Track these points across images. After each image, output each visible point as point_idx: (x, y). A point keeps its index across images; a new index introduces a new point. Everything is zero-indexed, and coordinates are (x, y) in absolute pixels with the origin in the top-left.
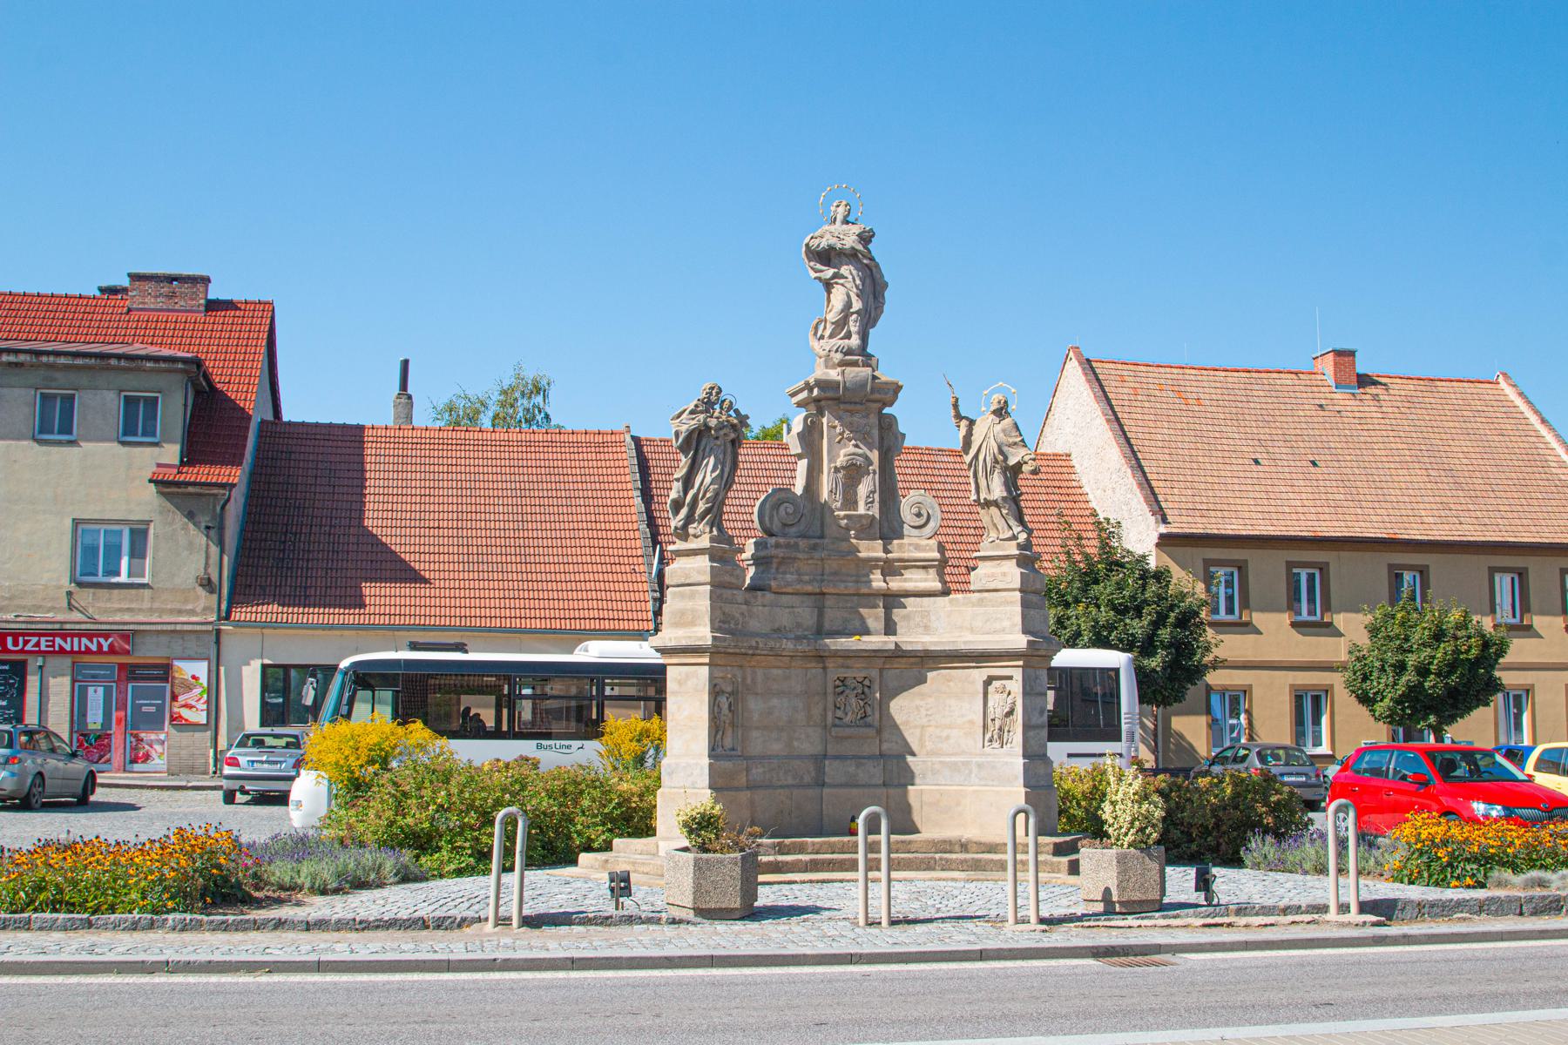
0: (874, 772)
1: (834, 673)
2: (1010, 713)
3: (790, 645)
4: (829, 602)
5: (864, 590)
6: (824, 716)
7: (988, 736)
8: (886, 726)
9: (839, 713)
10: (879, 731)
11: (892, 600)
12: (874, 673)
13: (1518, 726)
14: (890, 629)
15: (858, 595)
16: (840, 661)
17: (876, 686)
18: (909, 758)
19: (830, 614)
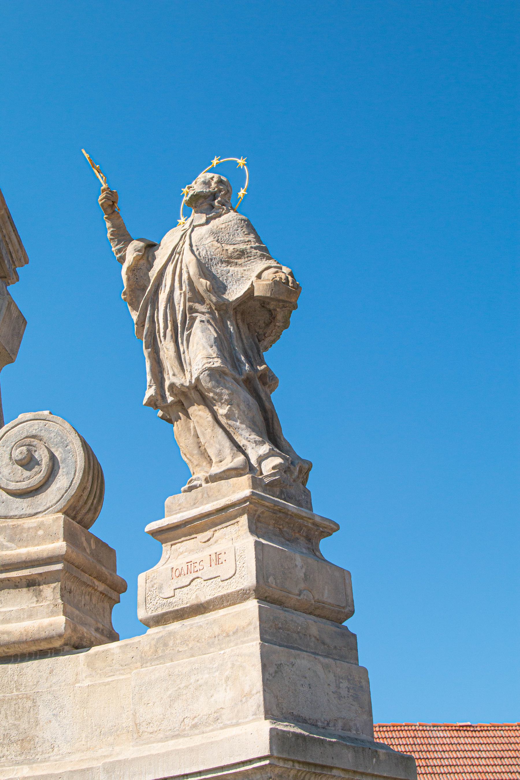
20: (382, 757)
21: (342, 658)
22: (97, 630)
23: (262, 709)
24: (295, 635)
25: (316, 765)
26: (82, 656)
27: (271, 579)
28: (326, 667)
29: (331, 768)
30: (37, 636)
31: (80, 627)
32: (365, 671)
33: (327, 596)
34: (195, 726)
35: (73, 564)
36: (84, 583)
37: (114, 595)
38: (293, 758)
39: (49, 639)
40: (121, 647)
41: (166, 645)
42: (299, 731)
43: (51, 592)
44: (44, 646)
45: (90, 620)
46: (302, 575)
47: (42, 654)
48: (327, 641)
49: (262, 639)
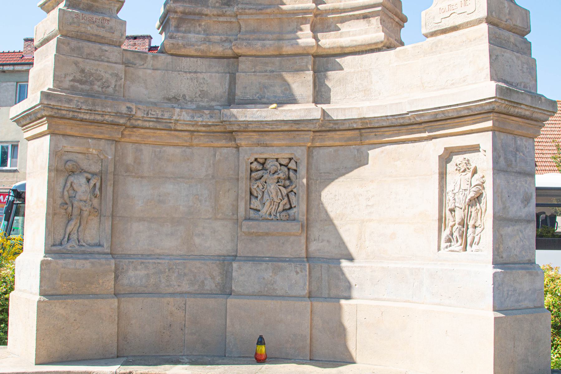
0: (295, 279)
1: (249, 153)
2: (477, 199)
3: (186, 116)
4: (244, 64)
5: (287, 49)
6: (236, 208)
7: (445, 234)
8: (315, 220)
9: (256, 204)
10: (307, 227)
11: (323, 62)
12: (300, 153)
13: (115, 264)
14: (320, 95)
15: (280, 55)
16: (255, 136)
17: (302, 171)
18: (345, 263)
19: (242, 79)
20: (543, 101)
21: (525, 53)
22: (396, 40)
23: (489, 76)
24: (504, 42)
25: (514, 102)
26: (392, 52)
27: (494, 13)
28: (518, 58)
29: (521, 104)
30: (370, 42)
31: (390, 38)
32: (535, 60)
33: (519, 23)
34: (453, 84)
35: (385, 7)
36: (390, 17)
37: (401, 23)
38: (505, 98)
39: (376, 44)
40: (412, 47)
41: (437, 46)
42: (505, 86)
43: (375, 21)
44: (373, 47)
45: (393, 35)
46: (508, 12)
47: (372, 51)
48: (518, 45)
49: (489, 43)
